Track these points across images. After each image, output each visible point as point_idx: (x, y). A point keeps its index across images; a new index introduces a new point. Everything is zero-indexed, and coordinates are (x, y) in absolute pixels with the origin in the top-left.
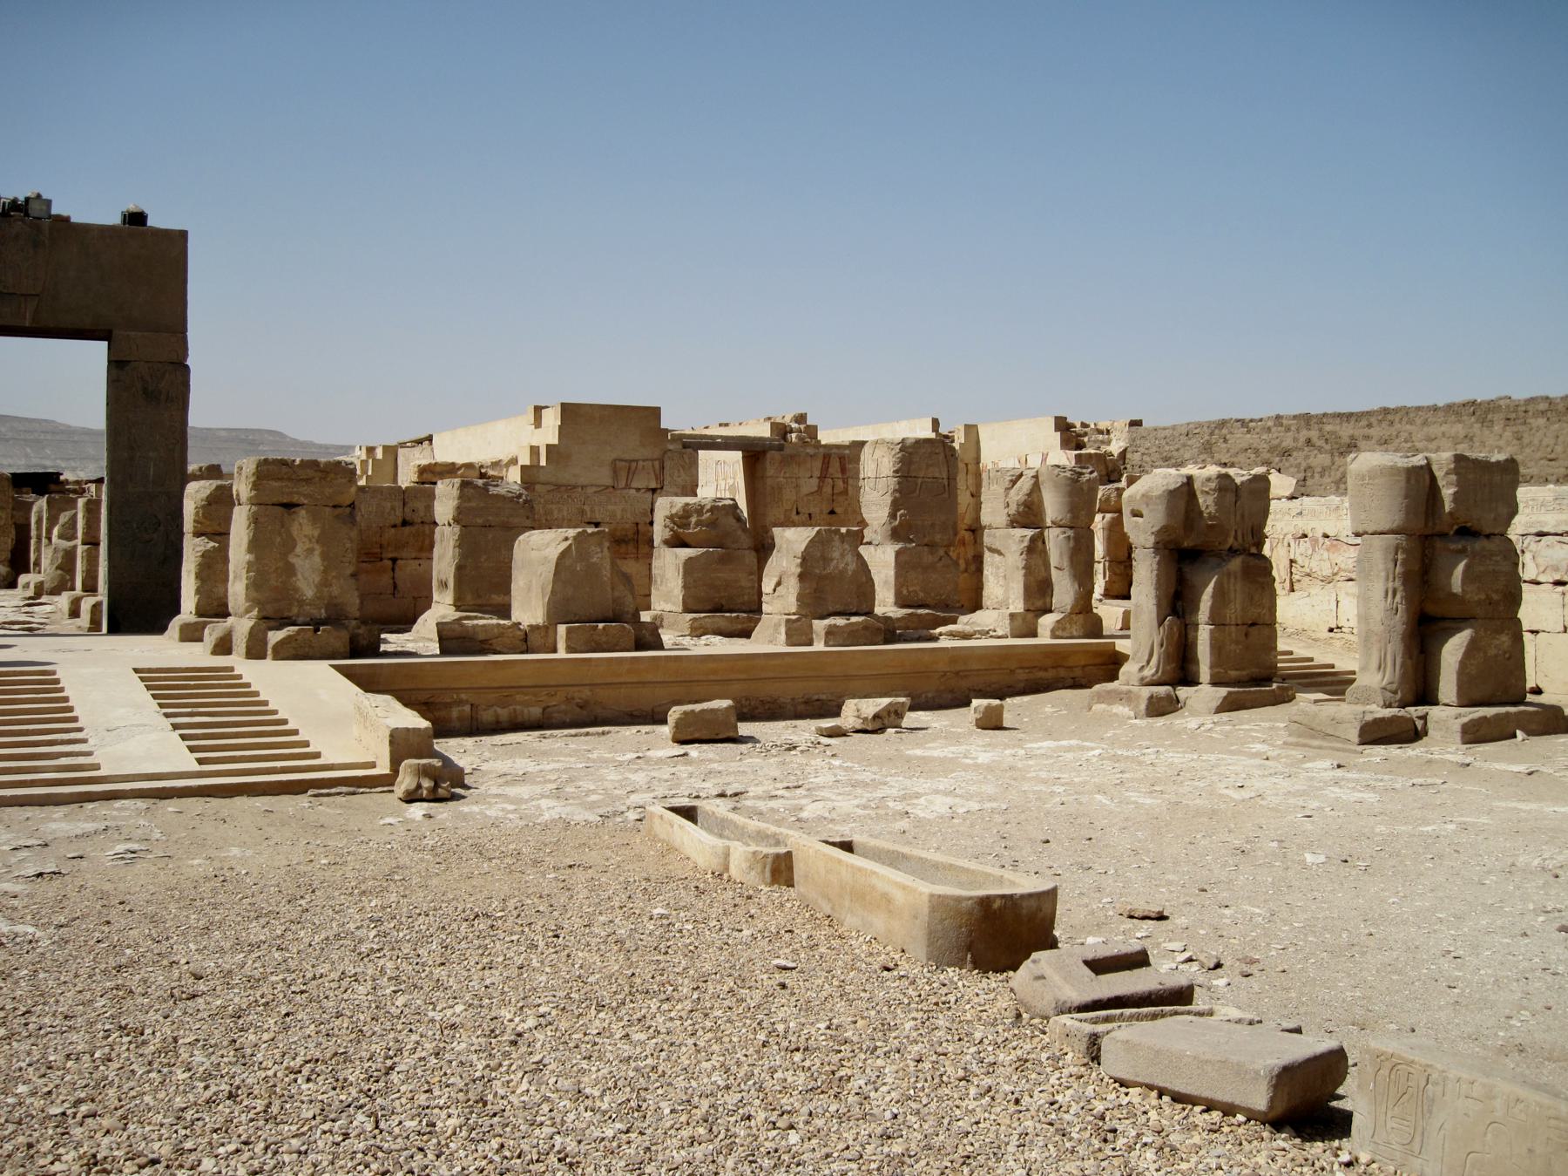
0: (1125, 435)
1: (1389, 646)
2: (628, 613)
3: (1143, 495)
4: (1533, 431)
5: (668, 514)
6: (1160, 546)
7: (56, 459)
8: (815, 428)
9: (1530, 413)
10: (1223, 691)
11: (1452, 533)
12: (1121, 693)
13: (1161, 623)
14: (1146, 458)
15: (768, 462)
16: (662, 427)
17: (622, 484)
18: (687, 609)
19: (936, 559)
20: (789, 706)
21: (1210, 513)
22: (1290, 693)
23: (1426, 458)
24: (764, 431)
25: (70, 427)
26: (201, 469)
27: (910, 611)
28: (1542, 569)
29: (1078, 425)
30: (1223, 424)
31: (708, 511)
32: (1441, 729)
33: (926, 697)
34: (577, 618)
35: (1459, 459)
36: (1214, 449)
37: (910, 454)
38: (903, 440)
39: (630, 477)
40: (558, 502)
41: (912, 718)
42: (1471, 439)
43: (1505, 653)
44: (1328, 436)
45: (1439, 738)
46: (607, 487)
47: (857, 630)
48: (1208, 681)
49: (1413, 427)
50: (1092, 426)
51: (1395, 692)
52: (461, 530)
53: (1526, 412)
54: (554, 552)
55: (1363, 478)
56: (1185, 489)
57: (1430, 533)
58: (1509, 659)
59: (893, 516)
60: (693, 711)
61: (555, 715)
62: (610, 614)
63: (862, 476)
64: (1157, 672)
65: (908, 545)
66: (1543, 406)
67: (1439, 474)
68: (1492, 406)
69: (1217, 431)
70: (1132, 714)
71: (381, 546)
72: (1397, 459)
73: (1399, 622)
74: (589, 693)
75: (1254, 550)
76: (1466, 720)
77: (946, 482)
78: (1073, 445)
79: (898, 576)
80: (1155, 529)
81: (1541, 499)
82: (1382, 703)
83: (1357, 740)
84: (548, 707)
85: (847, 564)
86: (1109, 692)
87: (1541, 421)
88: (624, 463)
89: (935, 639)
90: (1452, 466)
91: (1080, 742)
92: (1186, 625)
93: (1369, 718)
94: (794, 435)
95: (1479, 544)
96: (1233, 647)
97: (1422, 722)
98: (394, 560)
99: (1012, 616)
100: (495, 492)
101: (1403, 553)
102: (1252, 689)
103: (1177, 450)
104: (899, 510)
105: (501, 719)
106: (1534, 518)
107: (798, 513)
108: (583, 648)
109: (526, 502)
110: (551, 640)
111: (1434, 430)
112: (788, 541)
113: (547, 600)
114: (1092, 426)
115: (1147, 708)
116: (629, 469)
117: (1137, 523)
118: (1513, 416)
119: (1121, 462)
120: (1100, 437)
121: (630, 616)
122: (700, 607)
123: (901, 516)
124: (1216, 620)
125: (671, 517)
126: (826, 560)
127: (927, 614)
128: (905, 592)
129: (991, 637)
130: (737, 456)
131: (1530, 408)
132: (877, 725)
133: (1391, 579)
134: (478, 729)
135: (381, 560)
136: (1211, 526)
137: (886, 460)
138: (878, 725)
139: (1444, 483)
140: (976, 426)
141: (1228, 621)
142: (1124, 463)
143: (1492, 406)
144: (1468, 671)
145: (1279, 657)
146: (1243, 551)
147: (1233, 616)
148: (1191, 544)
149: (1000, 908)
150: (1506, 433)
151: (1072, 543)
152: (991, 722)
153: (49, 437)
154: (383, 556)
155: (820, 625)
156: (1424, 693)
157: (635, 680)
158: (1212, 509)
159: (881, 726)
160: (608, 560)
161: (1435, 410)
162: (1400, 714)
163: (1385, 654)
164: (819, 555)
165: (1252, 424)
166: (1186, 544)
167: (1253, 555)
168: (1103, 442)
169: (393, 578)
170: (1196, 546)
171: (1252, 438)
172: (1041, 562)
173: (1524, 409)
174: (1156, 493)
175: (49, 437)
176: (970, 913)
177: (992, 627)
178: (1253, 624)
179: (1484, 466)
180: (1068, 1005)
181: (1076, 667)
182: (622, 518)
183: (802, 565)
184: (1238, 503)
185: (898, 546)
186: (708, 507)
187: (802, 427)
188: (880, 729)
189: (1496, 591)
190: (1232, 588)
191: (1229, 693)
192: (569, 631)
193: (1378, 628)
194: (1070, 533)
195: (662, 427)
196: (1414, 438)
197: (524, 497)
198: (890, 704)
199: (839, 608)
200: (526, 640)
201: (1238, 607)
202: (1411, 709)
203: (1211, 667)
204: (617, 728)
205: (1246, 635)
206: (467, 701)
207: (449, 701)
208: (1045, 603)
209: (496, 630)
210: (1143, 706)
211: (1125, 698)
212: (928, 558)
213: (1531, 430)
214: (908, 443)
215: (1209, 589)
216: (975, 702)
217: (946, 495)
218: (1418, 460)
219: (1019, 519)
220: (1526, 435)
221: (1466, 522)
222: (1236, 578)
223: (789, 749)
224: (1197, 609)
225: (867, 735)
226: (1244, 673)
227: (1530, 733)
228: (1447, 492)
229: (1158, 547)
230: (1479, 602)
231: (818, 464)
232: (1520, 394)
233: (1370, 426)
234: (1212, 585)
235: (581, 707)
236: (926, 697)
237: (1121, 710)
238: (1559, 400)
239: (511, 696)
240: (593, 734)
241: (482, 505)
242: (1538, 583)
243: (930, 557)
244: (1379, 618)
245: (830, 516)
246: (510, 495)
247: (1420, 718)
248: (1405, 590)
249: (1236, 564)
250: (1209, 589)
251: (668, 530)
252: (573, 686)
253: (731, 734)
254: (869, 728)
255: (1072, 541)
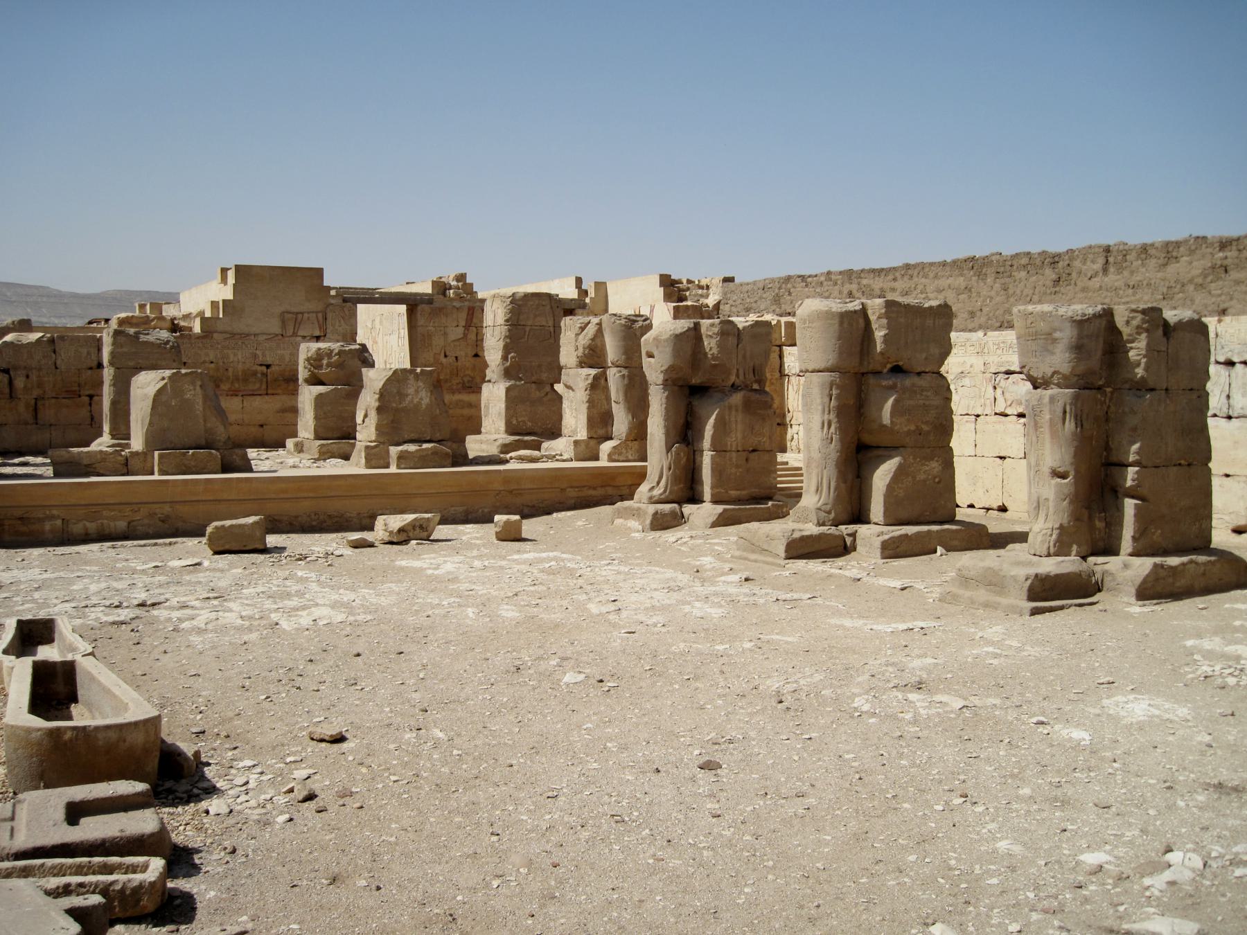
0: (719, 290)
1: (825, 471)
2: (219, 441)
3: (654, 339)
4: (1017, 283)
5: (306, 357)
6: (669, 382)
7: (50, 317)
8: (471, 285)
9: (1015, 267)
10: (720, 508)
11: (885, 371)
12: (633, 509)
13: (668, 450)
14: (734, 309)
15: (419, 313)
16: (325, 284)
17: (290, 332)
18: (318, 437)
19: (543, 395)
20: (355, 520)
21: (713, 354)
22: (785, 510)
23: (863, 304)
24: (426, 288)
25: (60, 291)
26: (13, 322)
27: (517, 438)
28: (1009, 403)
29: (685, 282)
30: (788, 279)
31: (336, 355)
32: (866, 546)
33: (483, 511)
34: (173, 445)
35: (890, 304)
36: (782, 301)
37: (519, 306)
38: (514, 294)
39: (297, 326)
40: (234, 348)
41: (442, 531)
42: (970, 291)
43: (935, 478)
44: (864, 289)
45: (864, 553)
46: (277, 335)
47: (427, 455)
48: (709, 500)
49: (927, 281)
50: (697, 283)
51: (829, 512)
52: (115, 372)
53: (1011, 266)
54: (152, 390)
55: (805, 320)
56: (692, 333)
57: (865, 371)
58: (939, 482)
59: (505, 358)
60: (223, 526)
61: (140, 528)
62: (203, 442)
63: (485, 325)
64: (665, 491)
65: (518, 383)
66: (1024, 261)
67: (873, 318)
68: (986, 261)
69: (784, 286)
70: (640, 528)
71: (79, 385)
72: (833, 305)
73: (834, 449)
74: (170, 510)
75: (756, 386)
76: (886, 537)
77: (552, 329)
78: (675, 298)
79: (508, 408)
80: (663, 368)
81: (1010, 342)
82: (816, 522)
83: (783, 555)
84: (133, 521)
85: (421, 399)
86: (626, 509)
87: (1023, 274)
88: (290, 315)
89: (507, 461)
90: (883, 311)
91: (537, 555)
92: (694, 451)
93: (797, 535)
94: (452, 291)
95: (908, 381)
96: (734, 470)
97: (851, 538)
98: (91, 397)
99: (576, 443)
100: (145, 340)
101: (837, 388)
102: (748, 507)
103: (756, 302)
104: (510, 353)
105: (90, 531)
106: (1004, 358)
107: (446, 356)
108: (174, 470)
109: (172, 347)
110: (149, 465)
111: (943, 283)
112: (371, 380)
113: (145, 430)
114: (697, 283)
115: (652, 523)
116: (296, 319)
117: (650, 362)
118: (1002, 269)
119: (716, 313)
120: (700, 292)
121: (221, 444)
122: (330, 435)
123: (512, 358)
124: (717, 447)
125: (308, 360)
126: (402, 396)
127: (533, 440)
128: (514, 422)
129: (557, 460)
130: (402, 308)
131: (1015, 263)
132: (401, 538)
133: (826, 412)
134: (69, 540)
135: (80, 396)
136: (715, 366)
137: (500, 311)
138: (403, 537)
139: (877, 326)
140: (605, 283)
141: (729, 448)
142: (718, 314)
143: (986, 261)
144: (895, 494)
145: (779, 479)
146: (746, 387)
147: (734, 444)
148: (699, 381)
149: (71, 740)
150: (997, 285)
151: (626, 381)
152: (511, 535)
153: (45, 299)
154: (81, 393)
155: (394, 451)
156: (859, 516)
157: (211, 498)
158: (715, 351)
159: (407, 539)
160: (201, 396)
161: (944, 265)
162: (829, 532)
163: (822, 479)
164: (395, 391)
165: (810, 279)
166: (693, 381)
167: (756, 390)
168: (702, 296)
169: (91, 411)
170: (702, 383)
171: (809, 291)
172: (603, 397)
173: (1010, 263)
174: (665, 337)
175: (45, 299)
176: (39, 744)
177: (559, 452)
178: (754, 451)
179: (917, 311)
180: (6, 851)
181: (624, 486)
182: (290, 361)
183: (379, 400)
184: (740, 346)
185: (508, 384)
186: (337, 351)
187: (460, 284)
188: (405, 541)
189: (927, 423)
190: (733, 419)
191: (725, 510)
192: (161, 456)
193: (816, 455)
194: (625, 372)
195: (325, 284)
196: (928, 290)
197: (171, 344)
198: (415, 519)
199: (413, 436)
200: (126, 464)
201: (739, 435)
202: (842, 527)
203: (712, 488)
204: (184, 539)
205: (747, 460)
206: (58, 517)
207: (41, 516)
208: (607, 432)
209: (99, 456)
210: (648, 522)
211: (635, 514)
212: (535, 394)
213: (1015, 282)
214: (518, 296)
215: (712, 421)
216: (497, 518)
217: (552, 341)
218: (855, 306)
219: (586, 360)
220: (1011, 286)
221: (897, 361)
222: (737, 410)
223: (300, 560)
224: (703, 437)
225: (394, 546)
226: (744, 493)
227: (949, 549)
228: (879, 334)
229: (666, 384)
230: (909, 433)
231: (463, 316)
232: (1008, 251)
233: (895, 280)
234: (714, 417)
235: (163, 521)
236: (483, 511)
237: (634, 524)
238: (1036, 256)
239: (99, 512)
240: (160, 545)
241: (134, 350)
242: (1006, 415)
243: (537, 392)
244: (817, 447)
245: (475, 358)
246: (158, 342)
247: (849, 535)
248: (838, 422)
249: (737, 398)
250: (712, 421)
251: (307, 370)
252: (153, 503)
253: (517, 537)
254: (395, 540)
255: (626, 379)
